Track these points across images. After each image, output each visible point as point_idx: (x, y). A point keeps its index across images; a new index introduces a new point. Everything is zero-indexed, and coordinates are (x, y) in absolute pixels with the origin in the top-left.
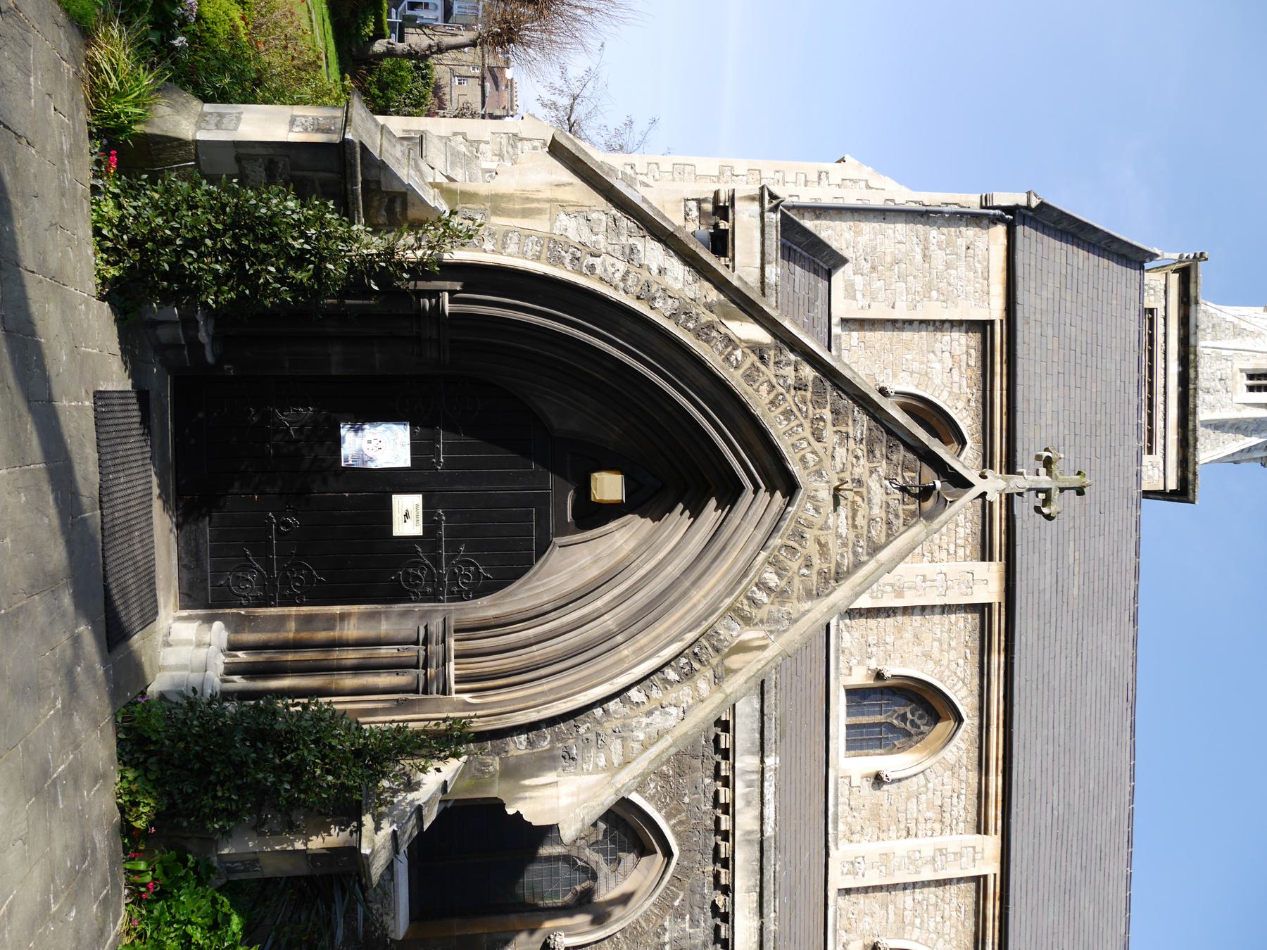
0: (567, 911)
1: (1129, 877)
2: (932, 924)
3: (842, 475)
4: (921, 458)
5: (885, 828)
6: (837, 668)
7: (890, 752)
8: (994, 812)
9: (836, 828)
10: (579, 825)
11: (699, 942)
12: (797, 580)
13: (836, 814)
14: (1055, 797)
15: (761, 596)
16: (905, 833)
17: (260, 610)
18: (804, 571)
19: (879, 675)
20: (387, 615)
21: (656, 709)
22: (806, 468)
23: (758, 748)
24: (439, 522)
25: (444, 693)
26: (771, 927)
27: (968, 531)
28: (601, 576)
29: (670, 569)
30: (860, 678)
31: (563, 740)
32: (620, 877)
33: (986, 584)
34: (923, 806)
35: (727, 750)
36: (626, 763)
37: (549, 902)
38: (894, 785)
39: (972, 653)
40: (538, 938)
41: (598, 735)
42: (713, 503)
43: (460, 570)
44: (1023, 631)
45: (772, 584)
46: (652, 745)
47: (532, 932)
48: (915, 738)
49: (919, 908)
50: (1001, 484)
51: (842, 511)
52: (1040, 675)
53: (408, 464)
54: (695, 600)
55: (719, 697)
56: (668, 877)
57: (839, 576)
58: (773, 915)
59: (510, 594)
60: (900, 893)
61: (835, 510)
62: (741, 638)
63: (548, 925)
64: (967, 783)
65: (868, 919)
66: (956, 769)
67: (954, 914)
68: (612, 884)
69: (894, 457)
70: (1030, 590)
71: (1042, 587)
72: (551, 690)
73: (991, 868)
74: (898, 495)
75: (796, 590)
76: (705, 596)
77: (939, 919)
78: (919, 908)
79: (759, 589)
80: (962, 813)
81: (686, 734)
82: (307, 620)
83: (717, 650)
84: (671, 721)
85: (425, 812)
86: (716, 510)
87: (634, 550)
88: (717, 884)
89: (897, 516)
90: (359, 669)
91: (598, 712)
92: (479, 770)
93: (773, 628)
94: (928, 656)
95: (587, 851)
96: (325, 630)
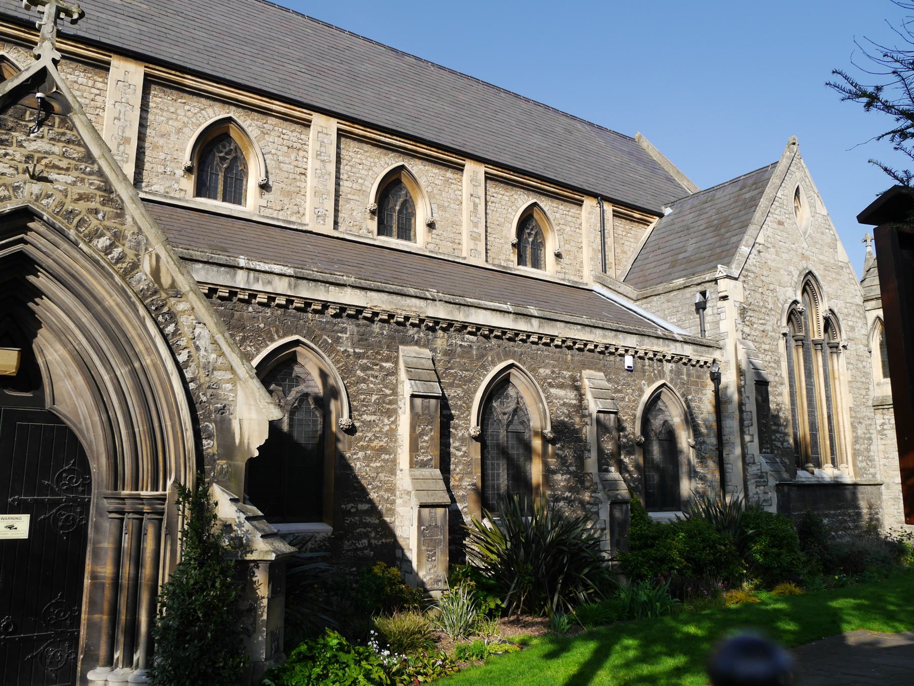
0: (326, 414)
1: (352, 34)
2: (363, 172)
3: (20, 170)
4: (14, 103)
5: (298, 189)
6: (179, 199)
7: (246, 174)
8: (297, 112)
9: (293, 223)
10: (272, 406)
11: (356, 329)
12: (107, 223)
13: (284, 221)
14: (293, 67)
15: (116, 252)
16: (303, 177)
17: (81, 643)
18: (100, 216)
19: (189, 170)
20: (95, 543)
21: (194, 343)
22: (10, 198)
23: (232, 270)
24: (19, 501)
25: (164, 500)
26: (352, 280)
27: (82, 74)
28: (83, 374)
29: (84, 320)
30: (189, 184)
31: (210, 413)
32: (309, 377)
33: (127, 74)
34: (287, 160)
35: (230, 292)
36: (232, 369)
37: (320, 427)
38: (270, 177)
39: (182, 98)
40: (341, 436)
41: (209, 387)
42: (31, 278)
43: (65, 484)
44: (170, 55)
45: (108, 243)
46: (221, 349)
47: (337, 440)
48: (239, 154)
49: (352, 179)
50: (47, 45)
51: (53, 176)
52: (205, 52)
53: (25, 535)
54: (113, 304)
55: (191, 296)
56: (312, 345)
57: (108, 189)
58: (345, 278)
59: (90, 445)
60: (342, 188)
61: (51, 182)
62: (148, 272)
63: (334, 429)
64: (275, 125)
65: (355, 213)
66: (265, 131)
67: (359, 156)
68: (312, 383)
69: (10, 124)
70: (138, 41)
71: (137, 31)
72: (171, 419)
73: (333, 125)
74: (44, 129)
75: (115, 225)
76: (111, 296)
77: (361, 167)
78: (352, 179)
79: (110, 253)
80: (295, 134)
81: (216, 324)
82: (94, 606)
83: (155, 292)
84: (205, 333)
85: (250, 514)
86: (38, 277)
87: (65, 346)
88: (321, 312)
89: (64, 134)
90: (138, 563)
91: (192, 386)
92: (225, 475)
93: (143, 248)
94: (179, 131)
95: (289, 398)
96: (103, 591)
